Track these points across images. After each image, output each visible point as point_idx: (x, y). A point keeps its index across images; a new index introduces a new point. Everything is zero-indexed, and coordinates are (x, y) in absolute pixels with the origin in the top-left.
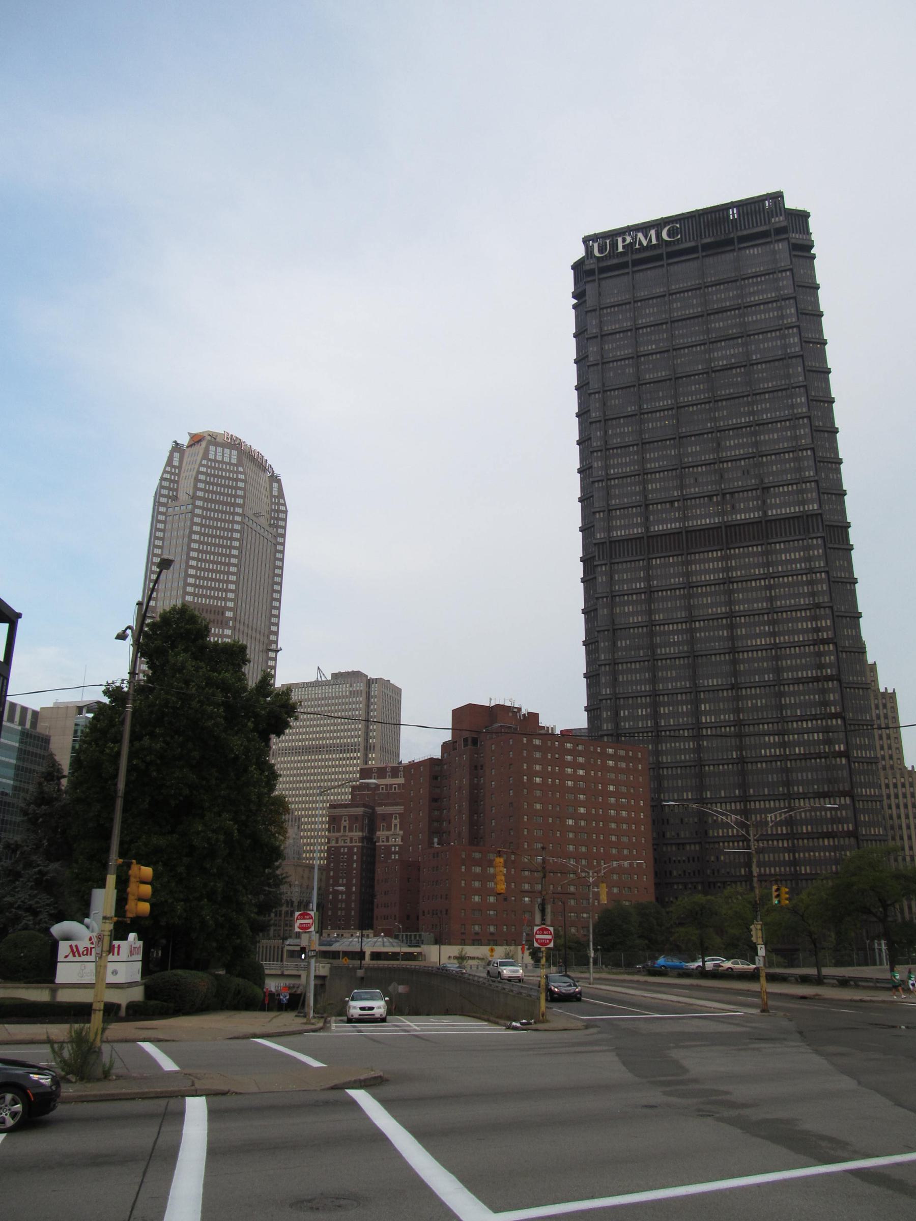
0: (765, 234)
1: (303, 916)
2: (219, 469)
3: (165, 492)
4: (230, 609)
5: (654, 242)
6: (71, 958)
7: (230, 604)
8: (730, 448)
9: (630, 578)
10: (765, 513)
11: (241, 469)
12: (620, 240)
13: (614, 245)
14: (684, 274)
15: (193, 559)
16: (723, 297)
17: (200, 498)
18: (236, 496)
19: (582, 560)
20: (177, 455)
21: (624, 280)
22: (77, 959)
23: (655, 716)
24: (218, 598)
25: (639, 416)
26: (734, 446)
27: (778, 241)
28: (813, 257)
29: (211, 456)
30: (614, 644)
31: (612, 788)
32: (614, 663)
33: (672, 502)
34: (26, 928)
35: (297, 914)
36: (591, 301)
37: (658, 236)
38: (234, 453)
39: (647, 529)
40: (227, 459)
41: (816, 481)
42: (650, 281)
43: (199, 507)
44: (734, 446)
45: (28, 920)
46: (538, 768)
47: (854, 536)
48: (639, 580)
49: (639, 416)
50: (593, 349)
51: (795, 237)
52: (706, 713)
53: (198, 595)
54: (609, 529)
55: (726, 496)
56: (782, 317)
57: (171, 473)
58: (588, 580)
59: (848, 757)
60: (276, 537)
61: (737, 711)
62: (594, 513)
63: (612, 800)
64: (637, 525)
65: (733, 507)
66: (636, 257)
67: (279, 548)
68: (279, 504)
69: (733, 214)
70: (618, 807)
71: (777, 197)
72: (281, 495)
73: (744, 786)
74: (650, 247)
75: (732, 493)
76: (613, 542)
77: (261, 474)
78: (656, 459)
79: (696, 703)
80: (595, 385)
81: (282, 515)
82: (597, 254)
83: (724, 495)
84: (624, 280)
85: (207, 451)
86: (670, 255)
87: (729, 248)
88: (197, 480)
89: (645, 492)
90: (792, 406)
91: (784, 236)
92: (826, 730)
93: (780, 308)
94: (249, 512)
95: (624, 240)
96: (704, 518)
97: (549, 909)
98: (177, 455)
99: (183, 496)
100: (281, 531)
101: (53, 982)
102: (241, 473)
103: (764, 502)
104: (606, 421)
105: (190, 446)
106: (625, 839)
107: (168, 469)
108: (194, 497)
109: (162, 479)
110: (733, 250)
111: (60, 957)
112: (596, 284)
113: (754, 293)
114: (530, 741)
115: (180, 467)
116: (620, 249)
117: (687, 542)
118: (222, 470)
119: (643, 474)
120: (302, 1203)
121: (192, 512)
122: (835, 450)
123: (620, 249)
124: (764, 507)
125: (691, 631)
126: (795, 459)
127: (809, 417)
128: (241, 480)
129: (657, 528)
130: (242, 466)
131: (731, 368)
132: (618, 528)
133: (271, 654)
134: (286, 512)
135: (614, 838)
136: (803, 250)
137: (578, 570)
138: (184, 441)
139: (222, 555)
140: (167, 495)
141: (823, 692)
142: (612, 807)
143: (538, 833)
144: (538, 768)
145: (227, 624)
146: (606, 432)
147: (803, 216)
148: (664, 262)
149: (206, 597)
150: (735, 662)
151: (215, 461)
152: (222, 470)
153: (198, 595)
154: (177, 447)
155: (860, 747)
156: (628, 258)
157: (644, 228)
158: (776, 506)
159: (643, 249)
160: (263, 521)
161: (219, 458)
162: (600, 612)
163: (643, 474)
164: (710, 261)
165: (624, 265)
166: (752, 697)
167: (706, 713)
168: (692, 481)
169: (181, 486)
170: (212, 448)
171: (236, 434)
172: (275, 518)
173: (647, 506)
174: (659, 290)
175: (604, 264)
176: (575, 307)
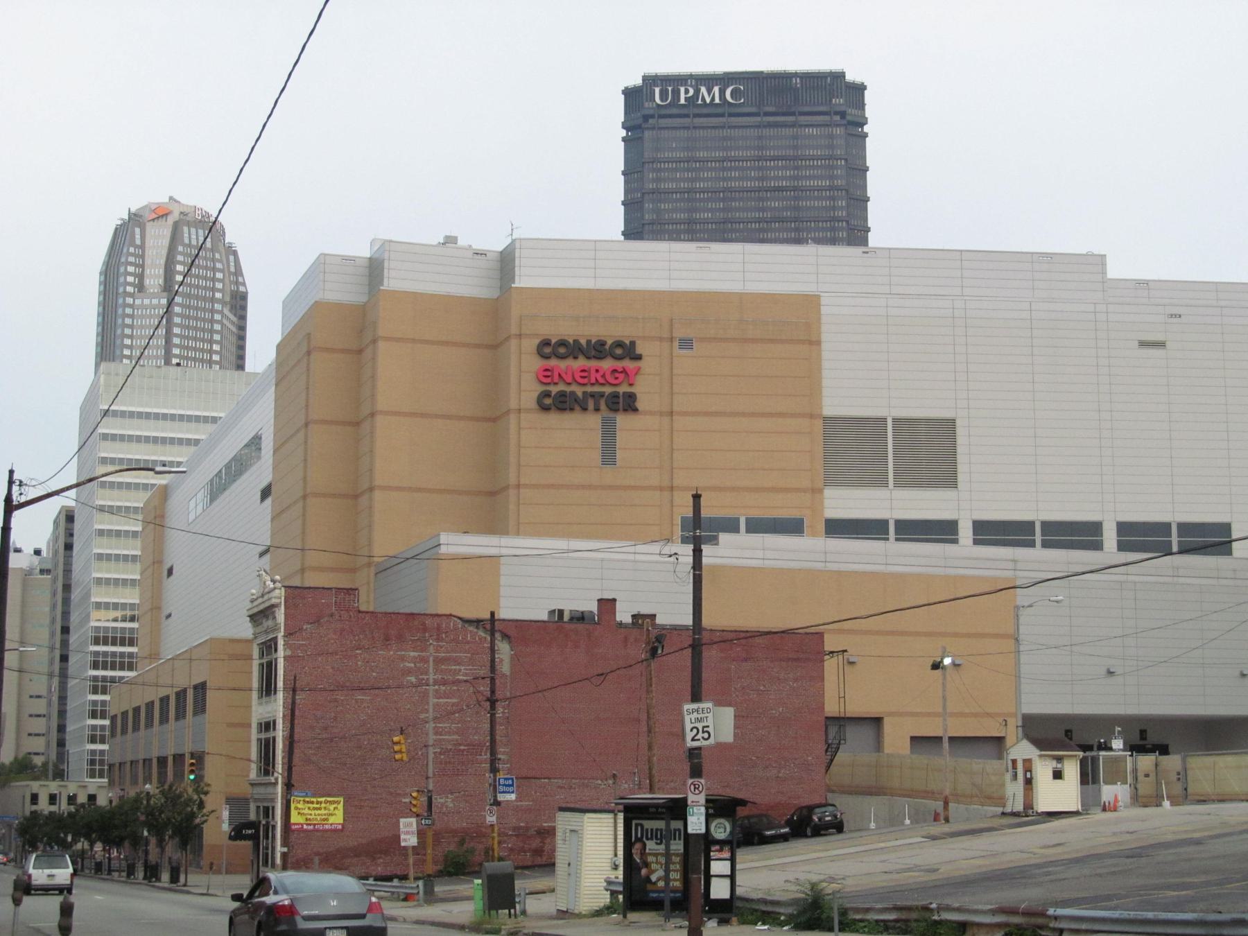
5: (717, 101)
12: (682, 90)
13: (676, 93)
28: (866, 135)
66: (696, 111)
72: (238, 272)
95: (687, 92)
115: (142, 247)
116: (682, 101)
120: (418, 922)
122: (866, 219)
123: (682, 101)
157: (709, 80)
175: (663, 112)
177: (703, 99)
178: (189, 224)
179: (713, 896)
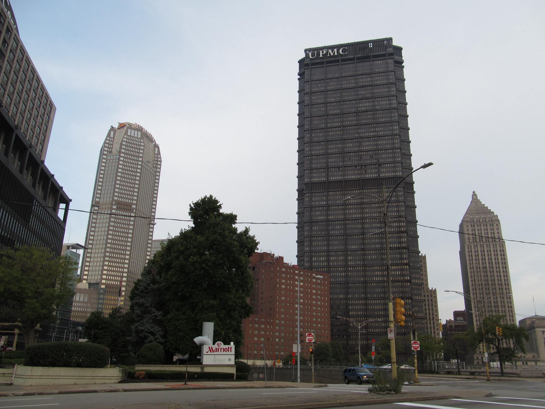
0: (384, 55)
1: (309, 335)
2: (132, 140)
3: (106, 149)
4: (134, 204)
5: (336, 54)
6: (209, 353)
7: (135, 202)
8: (365, 146)
9: (319, 200)
10: (379, 175)
11: (142, 141)
12: (321, 52)
14: (349, 69)
15: (118, 180)
16: (365, 81)
17: (123, 153)
18: (139, 153)
19: (298, 190)
20: (112, 133)
21: (323, 71)
22: (212, 353)
23: (328, 261)
24: (129, 199)
25: (326, 129)
26: (367, 145)
27: (390, 59)
28: (403, 67)
29: (129, 134)
30: (311, 228)
31: (314, 291)
32: (311, 236)
33: (339, 168)
34: (151, 342)
35: (307, 334)
36: (307, 77)
37: (338, 52)
38: (139, 133)
39: (328, 179)
40: (136, 136)
41: (402, 163)
42: (333, 71)
43: (122, 157)
44: (367, 145)
45: (151, 338)
46: (284, 281)
47: (416, 187)
48: (324, 201)
49: (326, 129)
50: (307, 98)
51: (396, 58)
52: (350, 260)
53: (120, 197)
54: (311, 177)
55: (363, 167)
56: (390, 91)
57: (109, 140)
58: (300, 199)
59: (411, 282)
60: (156, 173)
61: (364, 260)
62: (305, 170)
63: (314, 297)
64: (323, 177)
65: (365, 171)
66: (328, 60)
67: (157, 177)
68: (158, 158)
69: (371, 45)
70: (317, 300)
71: (390, 40)
73: (365, 293)
74: (334, 56)
75: (365, 166)
76: (313, 183)
77: (150, 143)
78: (333, 148)
79: (346, 256)
80: (307, 114)
81: (159, 163)
82: (310, 57)
83: (362, 166)
84: (323, 71)
85: (127, 132)
86: (343, 60)
87: (368, 60)
88: (121, 144)
89: (327, 163)
90: (393, 130)
91: (392, 57)
92: (402, 270)
93: (389, 87)
94: (145, 160)
95: (323, 52)
96: (352, 175)
97: (416, 334)
98: (112, 133)
99: (114, 151)
100: (158, 170)
101: (201, 364)
102: (142, 142)
103: (379, 170)
104: (311, 130)
105: (119, 128)
106: (319, 314)
107: (108, 138)
108: (120, 152)
109: (105, 143)
110: (370, 61)
111: (205, 353)
112: (310, 70)
113: (378, 80)
114: (281, 269)
115: (114, 138)
116: (321, 56)
117: (344, 185)
118: (133, 140)
119: (327, 155)
121: (119, 159)
122: (409, 150)
123: (321, 56)
124: (379, 172)
125: (346, 225)
126: (393, 153)
127: (399, 135)
128: (142, 146)
129: (332, 179)
130: (143, 139)
131: (367, 112)
132: (314, 177)
133: (151, 226)
134: (161, 161)
135: (314, 314)
136: (399, 63)
137: (296, 195)
138: (116, 126)
139: (132, 179)
140: (107, 151)
141: (401, 254)
142: (314, 300)
143: (283, 310)
144: (284, 281)
145: (133, 211)
146: (311, 135)
147: (399, 49)
148: (325, 65)
149: (124, 198)
150: (363, 239)
151: (130, 136)
152: (133, 140)
153: (120, 197)
154: (112, 128)
155: (415, 278)
156: (324, 60)
157: (332, 48)
158: (384, 172)
159: (331, 56)
160: (150, 165)
161: (132, 135)
162: (305, 214)
163: (327, 155)
164: (329, 68)
165: (322, 63)
166: (370, 254)
167: (350, 260)
168: (348, 158)
169: (114, 146)
170: (129, 130)
171: (141, 124)
172: (156, 164)
173: (328, 168)
174: (337, 75)
176: (299, 79)
177: (330, 54)
178: (131, 129)
179: (65, 205)
